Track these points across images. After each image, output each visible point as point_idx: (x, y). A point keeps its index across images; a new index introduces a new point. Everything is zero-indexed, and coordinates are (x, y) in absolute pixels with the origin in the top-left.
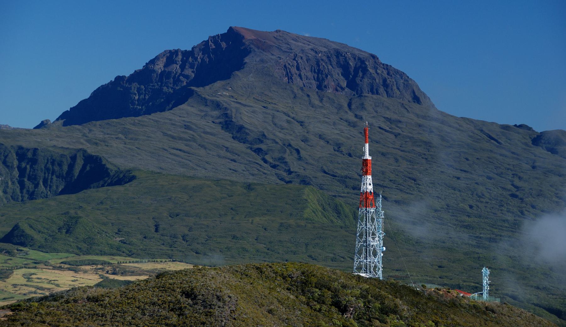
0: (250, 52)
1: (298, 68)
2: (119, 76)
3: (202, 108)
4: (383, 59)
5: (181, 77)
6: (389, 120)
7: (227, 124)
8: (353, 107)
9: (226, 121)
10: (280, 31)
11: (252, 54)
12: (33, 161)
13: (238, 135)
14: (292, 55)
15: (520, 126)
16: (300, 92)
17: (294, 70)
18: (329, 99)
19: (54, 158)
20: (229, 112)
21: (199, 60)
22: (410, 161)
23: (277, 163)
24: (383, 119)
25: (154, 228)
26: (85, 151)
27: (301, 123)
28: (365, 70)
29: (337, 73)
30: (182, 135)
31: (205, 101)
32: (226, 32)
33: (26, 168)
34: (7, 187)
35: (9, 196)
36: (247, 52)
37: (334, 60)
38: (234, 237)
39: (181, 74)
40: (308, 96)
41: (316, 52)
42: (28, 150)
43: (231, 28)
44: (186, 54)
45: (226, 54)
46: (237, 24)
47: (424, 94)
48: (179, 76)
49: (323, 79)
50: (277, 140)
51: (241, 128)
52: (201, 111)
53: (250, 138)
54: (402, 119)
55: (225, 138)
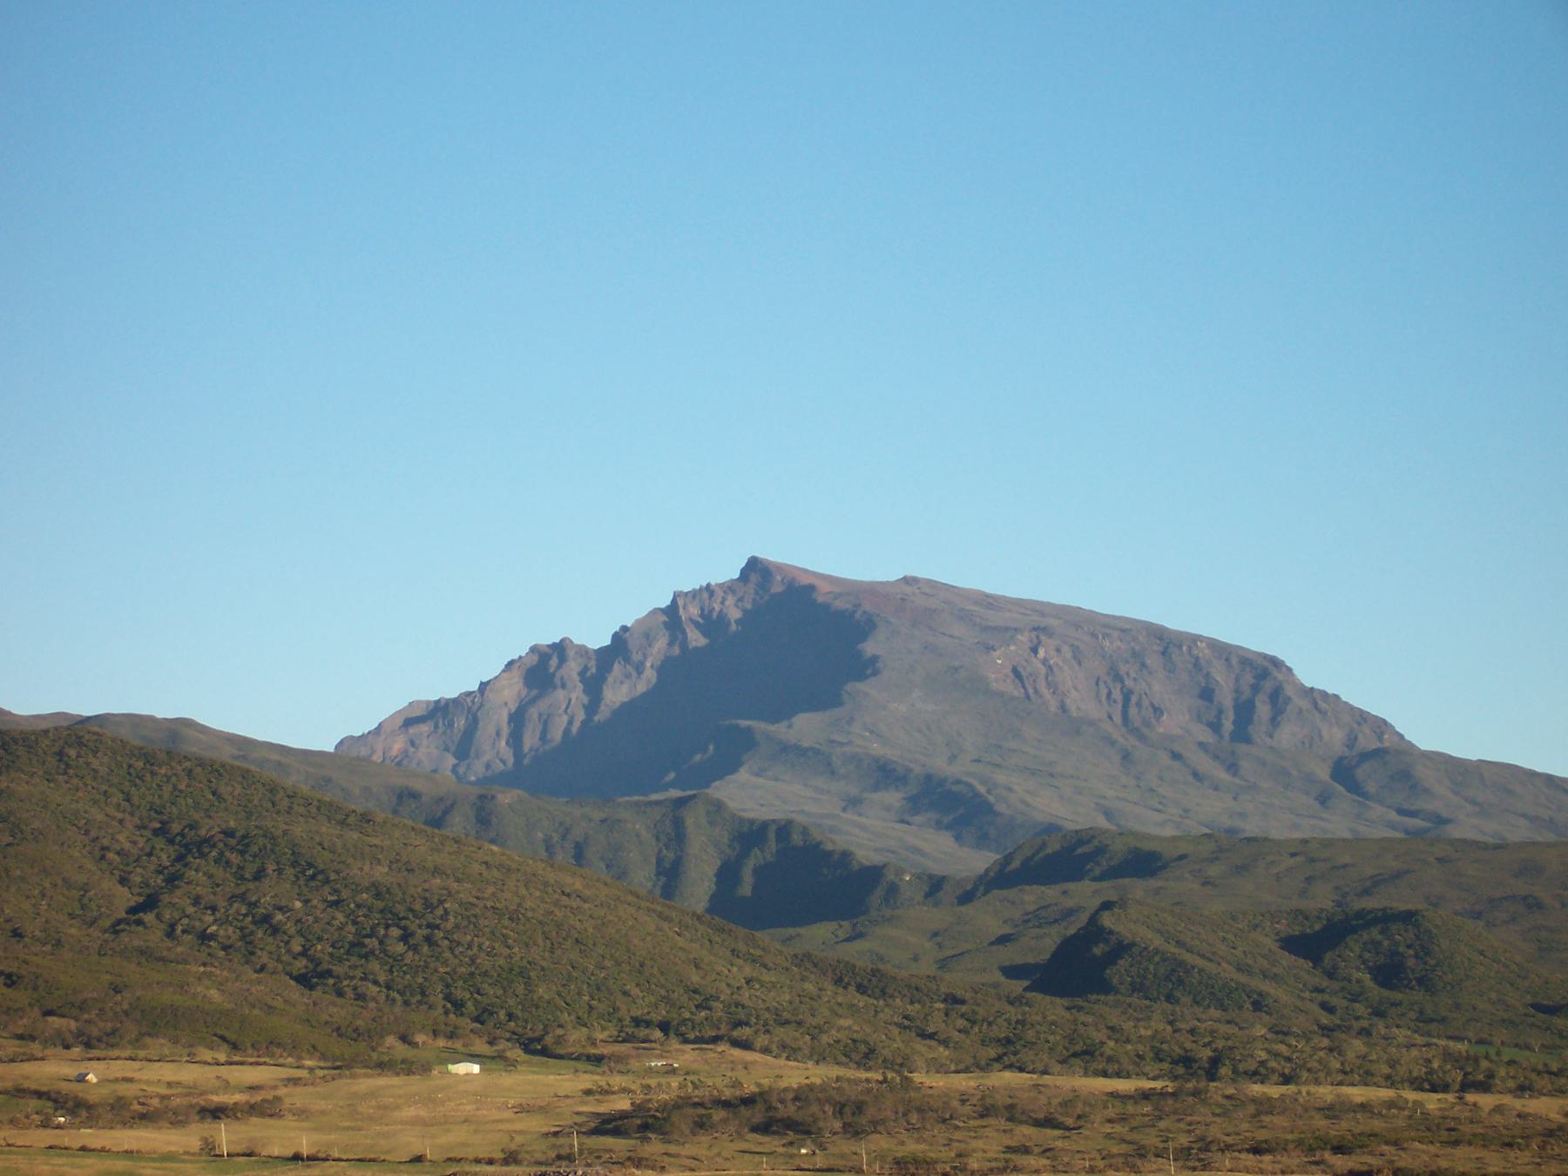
8: (1371, 787)
14: (1023, 638)
37: (1153, 661)
41: (1094, 635)
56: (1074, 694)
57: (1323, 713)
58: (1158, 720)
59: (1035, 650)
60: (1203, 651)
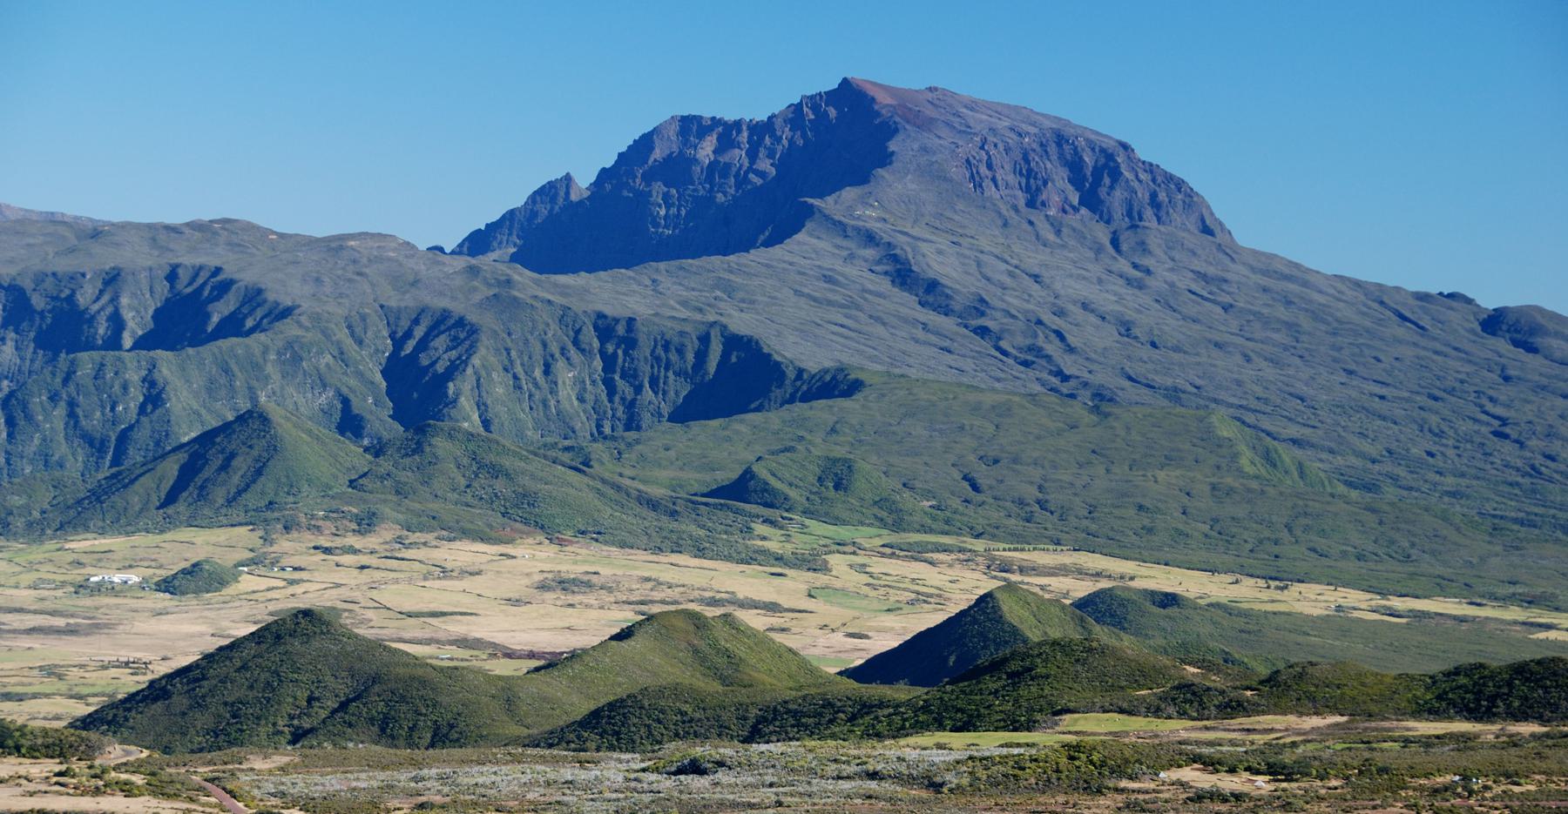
0: (896, 131)
1: (990, 167)
2: (604, 169)
3: (840, 241)
4: (1142, 153)
5: (751, 176)
6: (1203, 277)
7: (903, 275)
8: (1124, 247)
9: (898, 271)
10: (936, 89)
12: (630, 343)
13: (931, 299)
14: (977, 139)
15: (1451, 296)
16: (1013, 213)
17: (983, 170)
18: (1074, 230)
19: (667, 337)
20: (898, 251)
21: (785, 142)
22: (1272, 361)
23: (1029, 358)
24: (1191, 275)
25: (966, 484)
26: (725, 327)
27: (1036, 278)
28: (1116, 174)
29: (1060, 177)
30: (831, 296)
31: (841, 228)
33: (615, 354)
34: (585, 390)
35: (589, 407)
36: (890, 131)
37: (1052, 149)
38: (1141, 507)
39: (750, 169)
40: (1031, 223)
42: (617, 321)
43: (845, 80)
44: (762, 130)
45: (845, 136)
46: (857, 74)
47: (1221, 224)
48: (746, 173)
49: (1038, 189)
50: (1014, 312)
51: (932, 286)
52: (838, 247)
53: (957, 307)
54: (1228, 276)
55: (904, 303)
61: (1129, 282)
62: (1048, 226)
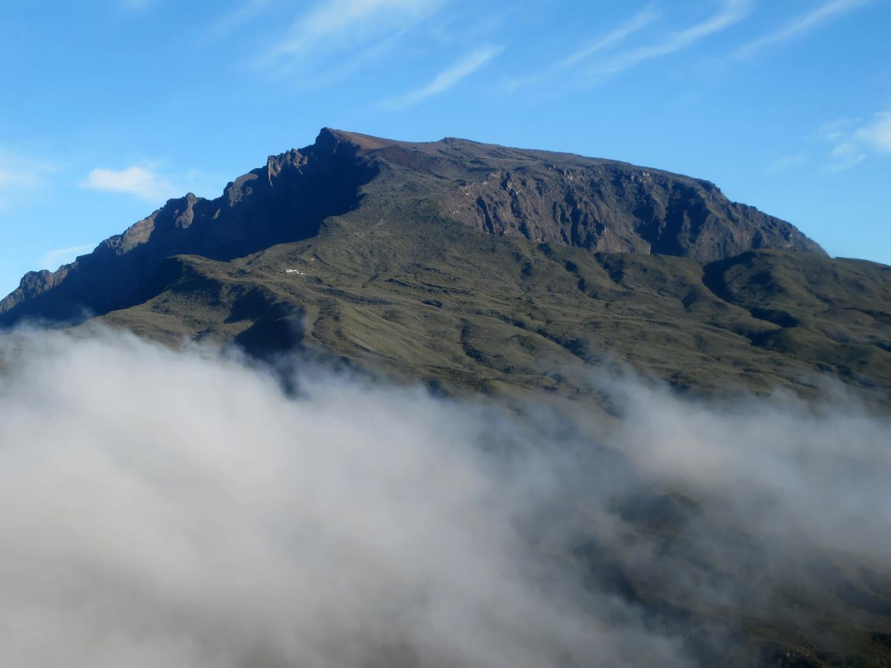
8: (735, 289)
11: (383, 174)
14: (497, 176)
16: (541, 256)
32: (313, 142)
37: (607, 189)
40: (571, 267)
41: (561, 172)
43: (325, 132)
56: (534, 217)
57: (736, 221)
58: (599, 234)
59: (504, 185)
60: (647, 180)
61: (759, 339)
62: (598, 267)
